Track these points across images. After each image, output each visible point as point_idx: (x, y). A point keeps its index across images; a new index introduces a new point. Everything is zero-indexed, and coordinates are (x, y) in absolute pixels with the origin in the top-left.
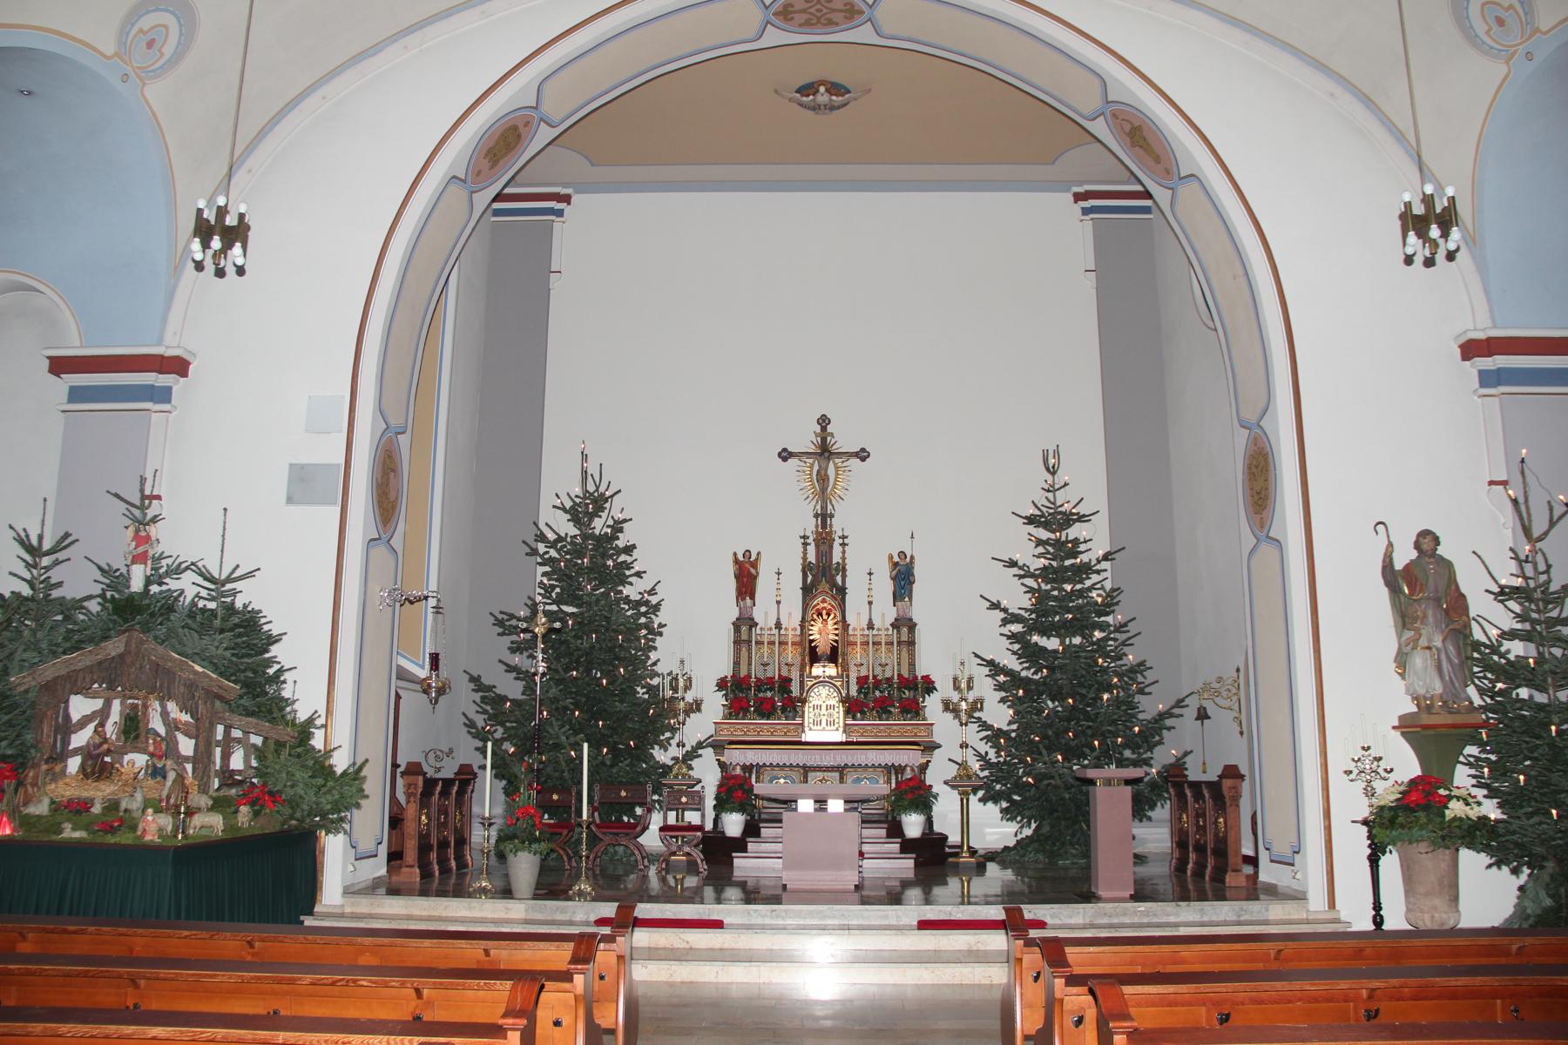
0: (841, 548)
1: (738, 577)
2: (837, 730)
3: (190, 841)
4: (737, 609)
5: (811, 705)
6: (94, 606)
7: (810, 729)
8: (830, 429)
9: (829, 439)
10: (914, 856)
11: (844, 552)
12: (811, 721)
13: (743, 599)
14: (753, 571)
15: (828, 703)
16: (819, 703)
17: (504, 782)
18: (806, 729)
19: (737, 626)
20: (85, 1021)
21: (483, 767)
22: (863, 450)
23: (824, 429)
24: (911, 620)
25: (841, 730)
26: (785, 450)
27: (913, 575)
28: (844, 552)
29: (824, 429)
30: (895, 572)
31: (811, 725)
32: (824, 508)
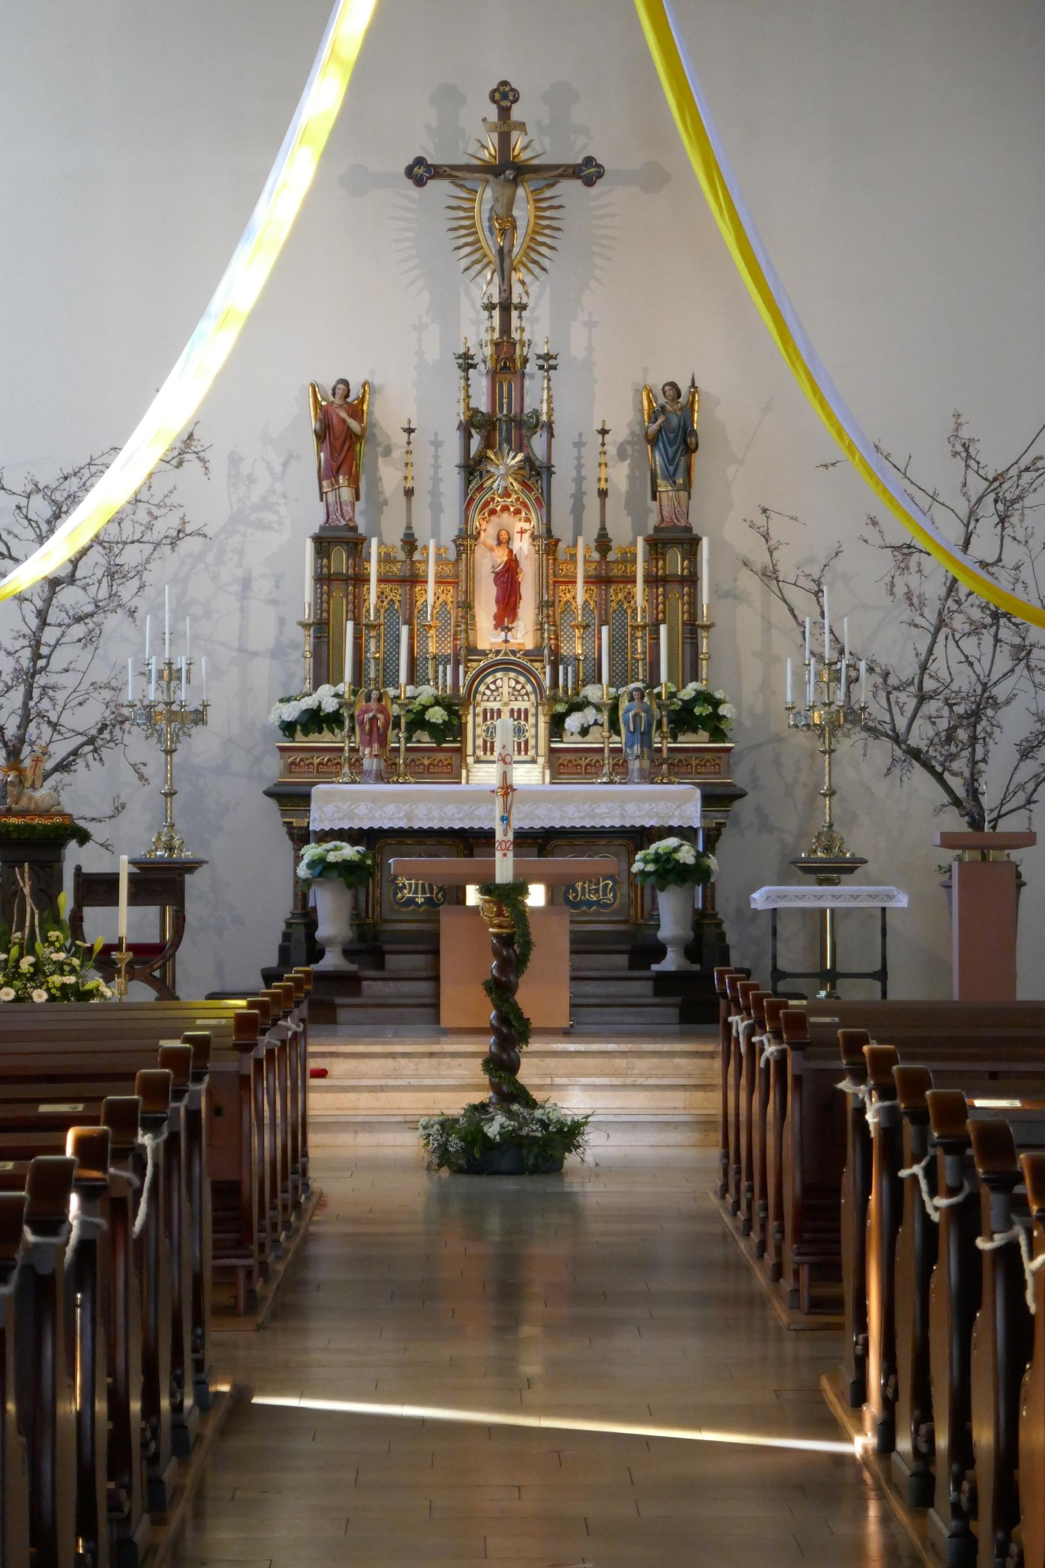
0: (431, 450)
1: (325, 432)
2: (533, 761)
3: (699, 661)
4: (322, 506)
5: (479, 710)
6: (498, 1138)
7: (478, 761)
8: (517, 113)
9: (515, 135)
10: (677, 1000)
11: (436, 457)
12: (480, 742)
13: (335, 487)
14: (354, 424)
15: (516, 705)
16: (496, 705)
17: (446, 1167)
18: (470, 760)
19: (323, 544)
20: (752, 274)
21: (138, 1193)
22: (589, 161)
23: (505, 113)
24: (688, 529)
25: (541, 760)
26: (420, 161)
27: (694, 433)
28: (436, 457)
29: (505, 113)
30: (654, 427)
31: (480, 753)
32: (506, 290)
